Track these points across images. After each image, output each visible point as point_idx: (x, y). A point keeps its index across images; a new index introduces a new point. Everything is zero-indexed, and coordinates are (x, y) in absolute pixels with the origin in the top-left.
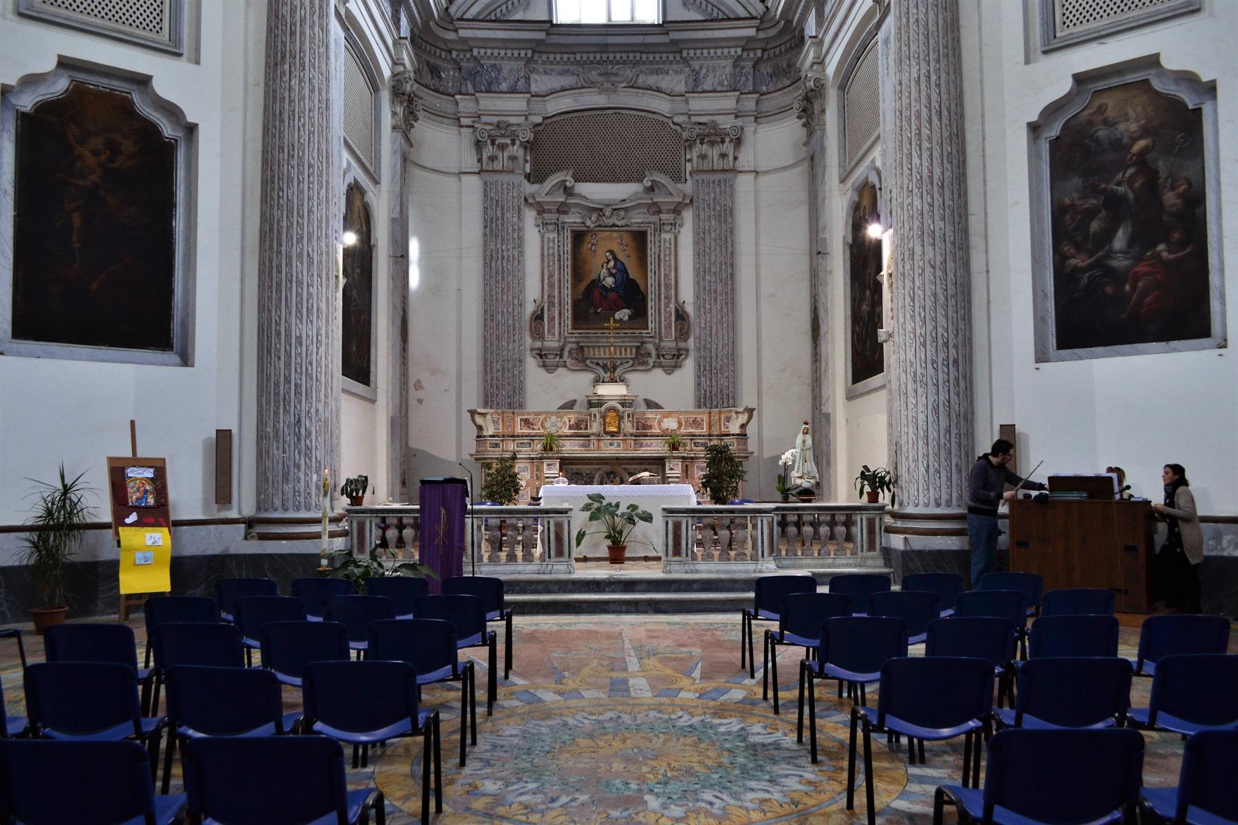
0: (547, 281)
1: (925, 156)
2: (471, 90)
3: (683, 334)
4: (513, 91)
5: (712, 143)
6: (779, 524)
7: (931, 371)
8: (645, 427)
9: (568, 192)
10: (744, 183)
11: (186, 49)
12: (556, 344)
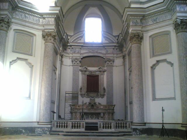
0: (83, 83)
1: (136, 71)
2: (71, 53)
3: (104, 92)
4: (78, 53)
5: (109, 62)
6: (116, 124)
7: (137, 102)
8: (98, 107)
9: (87, 69)
10: (114, 68)
11: (33, 55)
12: (84, 93)
